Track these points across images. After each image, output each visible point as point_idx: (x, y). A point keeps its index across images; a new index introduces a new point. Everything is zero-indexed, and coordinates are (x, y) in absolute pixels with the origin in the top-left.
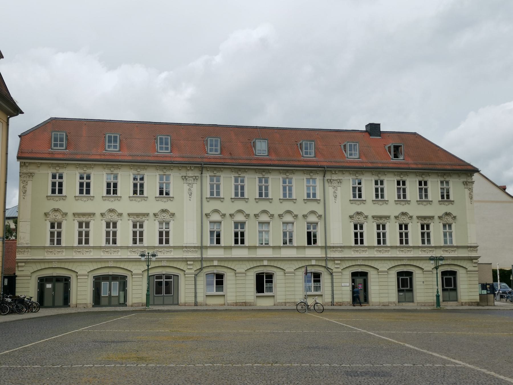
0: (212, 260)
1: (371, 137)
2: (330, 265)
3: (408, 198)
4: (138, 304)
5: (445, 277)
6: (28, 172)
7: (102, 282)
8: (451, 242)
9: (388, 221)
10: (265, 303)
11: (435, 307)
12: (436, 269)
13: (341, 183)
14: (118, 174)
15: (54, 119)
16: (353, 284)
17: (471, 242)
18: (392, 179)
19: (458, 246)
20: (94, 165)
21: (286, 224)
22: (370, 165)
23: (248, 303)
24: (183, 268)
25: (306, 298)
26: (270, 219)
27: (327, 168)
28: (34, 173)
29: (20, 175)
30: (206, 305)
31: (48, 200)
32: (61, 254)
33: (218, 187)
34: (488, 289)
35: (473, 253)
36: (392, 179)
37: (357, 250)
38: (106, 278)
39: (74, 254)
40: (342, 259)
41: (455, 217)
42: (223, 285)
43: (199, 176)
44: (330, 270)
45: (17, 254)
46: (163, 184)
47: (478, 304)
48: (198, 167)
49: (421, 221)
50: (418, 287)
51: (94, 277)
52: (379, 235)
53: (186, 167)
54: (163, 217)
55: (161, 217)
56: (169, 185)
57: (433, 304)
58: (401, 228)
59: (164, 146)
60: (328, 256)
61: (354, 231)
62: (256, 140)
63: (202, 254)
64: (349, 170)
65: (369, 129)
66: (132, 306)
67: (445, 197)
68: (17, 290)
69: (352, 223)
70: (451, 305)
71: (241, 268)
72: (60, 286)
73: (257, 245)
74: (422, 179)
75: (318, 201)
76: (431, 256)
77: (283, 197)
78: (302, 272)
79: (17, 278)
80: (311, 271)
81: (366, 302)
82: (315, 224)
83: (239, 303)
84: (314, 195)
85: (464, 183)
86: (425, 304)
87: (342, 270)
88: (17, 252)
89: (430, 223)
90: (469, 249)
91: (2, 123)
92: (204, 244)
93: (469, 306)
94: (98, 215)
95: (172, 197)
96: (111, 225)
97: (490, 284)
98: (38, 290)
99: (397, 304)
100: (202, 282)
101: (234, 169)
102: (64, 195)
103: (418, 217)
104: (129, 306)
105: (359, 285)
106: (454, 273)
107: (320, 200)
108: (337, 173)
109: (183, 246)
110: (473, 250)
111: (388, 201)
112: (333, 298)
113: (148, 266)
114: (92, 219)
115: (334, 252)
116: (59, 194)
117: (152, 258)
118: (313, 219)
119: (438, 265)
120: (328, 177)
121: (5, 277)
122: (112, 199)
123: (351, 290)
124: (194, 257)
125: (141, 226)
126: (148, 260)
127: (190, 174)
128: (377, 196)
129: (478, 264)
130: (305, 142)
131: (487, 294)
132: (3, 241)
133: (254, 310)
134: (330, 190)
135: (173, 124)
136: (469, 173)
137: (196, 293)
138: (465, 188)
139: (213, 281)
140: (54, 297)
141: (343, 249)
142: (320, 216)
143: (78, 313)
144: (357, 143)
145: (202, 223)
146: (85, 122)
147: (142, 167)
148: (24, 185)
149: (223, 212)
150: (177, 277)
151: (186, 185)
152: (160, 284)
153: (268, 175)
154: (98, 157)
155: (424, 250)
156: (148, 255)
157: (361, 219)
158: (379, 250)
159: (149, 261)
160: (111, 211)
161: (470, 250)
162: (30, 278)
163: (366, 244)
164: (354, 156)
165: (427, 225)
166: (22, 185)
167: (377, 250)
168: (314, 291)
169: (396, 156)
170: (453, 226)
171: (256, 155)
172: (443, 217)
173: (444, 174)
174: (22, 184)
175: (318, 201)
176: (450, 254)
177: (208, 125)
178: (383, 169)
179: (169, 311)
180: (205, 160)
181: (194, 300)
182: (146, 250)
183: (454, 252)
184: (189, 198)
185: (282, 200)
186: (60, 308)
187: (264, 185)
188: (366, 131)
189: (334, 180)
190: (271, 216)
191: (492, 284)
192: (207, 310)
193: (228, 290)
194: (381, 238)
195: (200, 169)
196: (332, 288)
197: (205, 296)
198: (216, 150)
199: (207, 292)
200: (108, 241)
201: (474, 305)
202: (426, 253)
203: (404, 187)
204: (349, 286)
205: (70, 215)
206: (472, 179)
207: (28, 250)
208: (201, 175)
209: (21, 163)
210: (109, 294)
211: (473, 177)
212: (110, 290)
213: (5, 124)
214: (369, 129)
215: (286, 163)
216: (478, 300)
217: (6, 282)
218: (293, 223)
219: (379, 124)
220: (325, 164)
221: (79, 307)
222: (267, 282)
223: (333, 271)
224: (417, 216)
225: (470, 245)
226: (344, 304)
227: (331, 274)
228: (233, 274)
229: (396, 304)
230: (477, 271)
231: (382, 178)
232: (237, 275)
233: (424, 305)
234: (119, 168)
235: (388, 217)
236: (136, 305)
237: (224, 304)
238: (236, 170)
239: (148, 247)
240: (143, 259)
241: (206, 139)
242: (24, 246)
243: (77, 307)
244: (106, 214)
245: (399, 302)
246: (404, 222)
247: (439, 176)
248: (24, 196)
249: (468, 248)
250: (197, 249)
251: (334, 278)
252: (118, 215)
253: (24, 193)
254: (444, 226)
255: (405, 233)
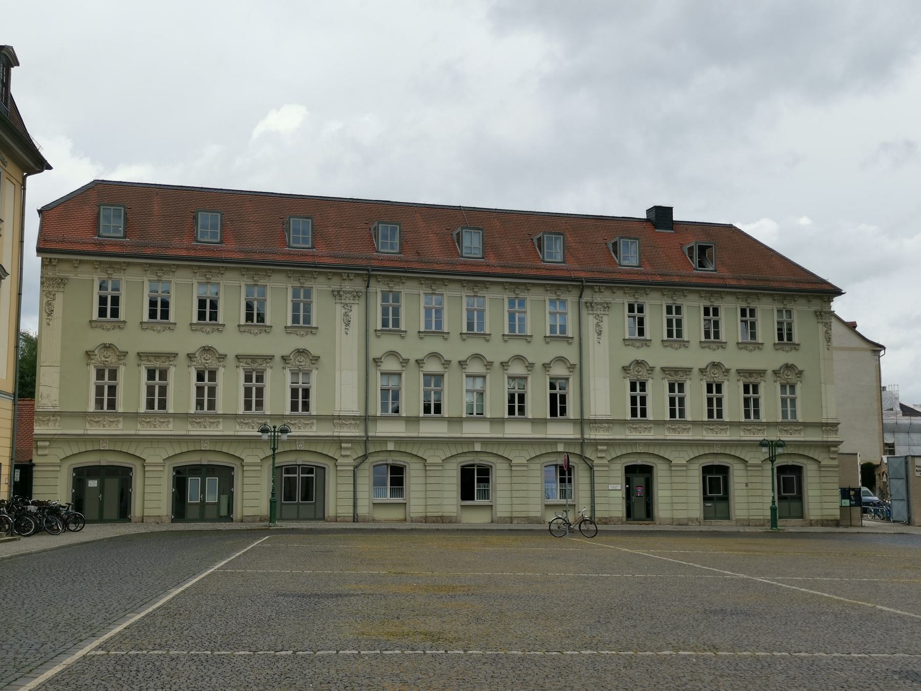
0: (384, 440)
1: (657, 230)
2: (589, 454)
3: (723, 337)
4: (253, 519)
5: (708, 477)
6: (56, 276)
7: (189, 478)
8: (794, 413)
9: (762, 378)
10: (477, 518)
11: (768, 528)
12: (771, 463)
13: (609, 308)
14: (401, 292)
15: (100, 182)
16: (627, 486)
17: (829, 415)
18: (458, 293)
19: (768, 423)
20: (176, 267)
21: (472, 378)
22: (659, 279)
23: (448, 517)
24: (328, 452)
25: (566, 511)
26: (401, 367)
27: (586, 282)
28: (68, 279)
29: (41, 282)
30: (374, 521)
31: (287, 333)
32: (165, 426)
33: (396, 312)
34: (852, 497)
35: (599, 432)
36: (696, 304)
37: (635, 426)
38: (196, 470)
39: (704, 433)
40: (610, 443)
41: (800, 373)
42: (403, 486)
43: (362, 290)
44: (589, 462)
45: (35, 425)
46: (515, 314)
47: (837, 523)
48: (362, 275)
49: (669, 377)
50: (737, 493)
51: (174, 468)
52: (633, 400)
53: (340, 274)
54: (204, 361)
55: (294, 362)
56: (310, 306)
57: (762, 522)
58: (710, 390)
59: (112, 225)
60: (586, 436)
61: (146, 383)
62: (378, 224)
63: (366, 431)
64: (623, 287)
65: (654, 216)
66: (242, 522)
67: (785, 335)
68: (35, 490)
69: (628, 379)
70: (790, 525)
71: (434, 456)
72: (113, 484)
73: (464, 416)
74: (709, 304)
75: (568, 340)
76: (762, 438)
77: (510, 332)
78: (620, 465)
79: (34, 469)
80: (555, 463)
81: (648, 519)
82: (564, 381)
83: (431, 518)
84: (563, 329)
85: (817, 314)
86: (748, 523)
87: (687, 462)
88: (36, 422)
89: (760, 383)
90: (824, 428)
91: (15, 185)
92: (371, 412)
93: (823, 526)
94: (182, 357)
95: (315, 327)
96: (714, 388)
97: (856, 490)
98: (74, 491)
99: (702, 522)
100: (366, 481)
101: (705, 292)
102: (122, 320)
103: (739, 372)
104: (237, 521)
105: (638, 488)
106: (798, 470)
107: (572, 338)
108: (602, 292)
109: (333, 416)
110: (830, 430)
111: (688, 342)
112: (593, 510)
113: (274, 450)
114: (171, 365)
115: (596, 430)
116: (100, 318)
117: (280, 436)
118: (559, 371)
119: (774, 454)
120: (587, 297)
121: (16, 467)
122: (208, 329)
123: (624, 496)
124: (353, 434)
125: (260, 379)
126: (274, 439)
127: (347, 287)
128: (670, 334)
129: (839, 454)
130: (293, 219)
131: (851, 505)
132: (14, 400)
133: (461, 530)
134: (590, 321)
135: (313, 198)
136: (827, 296)
137: (355, 499)
138: (818, 322)
139: (386, 478)
140: (101, 503)
141: (611, 425)
142: (572, 367)
143: (151, 532)
144: (635, 239)
145: (367, 375)
146: (157, 189)
147: (214, 271)
148: (49, 299)
149: (405, 356)
150: (323, 470)
151: (339, 307)
152: (290, 483)
153: (483, 292)
154: (184, 253)
155: (749, 428)
156: (275, 430)
157: (643, 375)
158: (673, 427)
159: (276, 441)
160: (207, 350)
161: (826, 430)
162: (58, 469)
163: (650, 416)
164: (114, 232)
165: (753, 385)
166: (45, 300)
167: (670, 428)
168: (560, 499)
169: (701, 265)
170: (798, 388)
171: (462, 257)
172: (631, 368)
173: (557, 288)
174: (45, 297)
175: (570, 341)
176: (791, 436)
177: (375, 202)
178: (681, 286)
179: (293, 531)
180: (375, 263)
181: (352, 512)
182: (268, 421)
183: (167, 425)
184: (596, 340)
185: (466, 336)
186: (113, 524)
187: (391, 305)
188: (647, 220)
189: (597, 304)
190: (530, 367)
191: (858, 490)
192: (378, 529)
193: (413, 495)
194: (676, 407)
195: (366, 279)
196: (591, 493)
197: (372, 505)
198: (305, 241)
199: (375, 498)
200: (200, 404)
201: (830, 526)
202: (752, 433)
203: (716, 318)
204: (620, 490)
205: (132, 356)
206: (830, 307)
207: (54, 418)
208: (367, 289)
209: (44, 260)
210: (201, 498)
211: (832, 303)
212: (203, 492)
213: (18, 187)
214: (653, 216)
215: (516, 272)
216: (838, 517)
217: (17, 475)
218: (400, 374)
219: (672, 208)
220: (583, 275)
221: (148, 521)
222: (479, 481)
223: (595, 463)
224: (737, 370)
225: (594, 418)
226: (613, 521)
227: (591, 468)
228: (420, 466)
229: (700, 523)
230: (837, 467)
231: (641, 300)
232: (673, 469)
233: (747, 523)
234: (173, 272)
235: (687, 371)
236: (249, 519)
237: (405, 520)
238: (429, 282)
239: (272, 417)
240: (265, 436)
241: (373, 227)
242: (48, 410)
243: (143, 522)
244: (197, 355)
245: (705, 518)
246: (715, 379)
247: (738, 298)
248: (828, 347)
249: (823, 427)
250: (358, 422)
251: (595, 475)
252: (219, 358)
253: (49, 315)
254: (783, 387)
255: (717, 398)
